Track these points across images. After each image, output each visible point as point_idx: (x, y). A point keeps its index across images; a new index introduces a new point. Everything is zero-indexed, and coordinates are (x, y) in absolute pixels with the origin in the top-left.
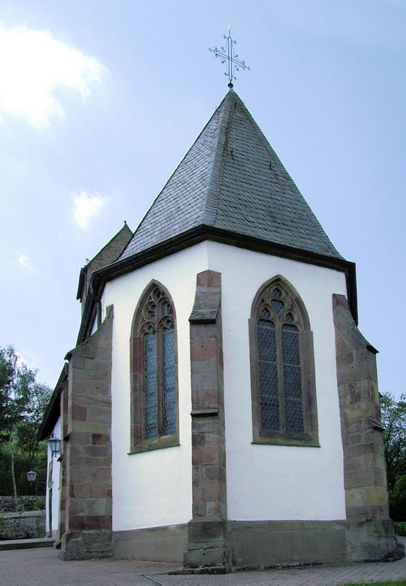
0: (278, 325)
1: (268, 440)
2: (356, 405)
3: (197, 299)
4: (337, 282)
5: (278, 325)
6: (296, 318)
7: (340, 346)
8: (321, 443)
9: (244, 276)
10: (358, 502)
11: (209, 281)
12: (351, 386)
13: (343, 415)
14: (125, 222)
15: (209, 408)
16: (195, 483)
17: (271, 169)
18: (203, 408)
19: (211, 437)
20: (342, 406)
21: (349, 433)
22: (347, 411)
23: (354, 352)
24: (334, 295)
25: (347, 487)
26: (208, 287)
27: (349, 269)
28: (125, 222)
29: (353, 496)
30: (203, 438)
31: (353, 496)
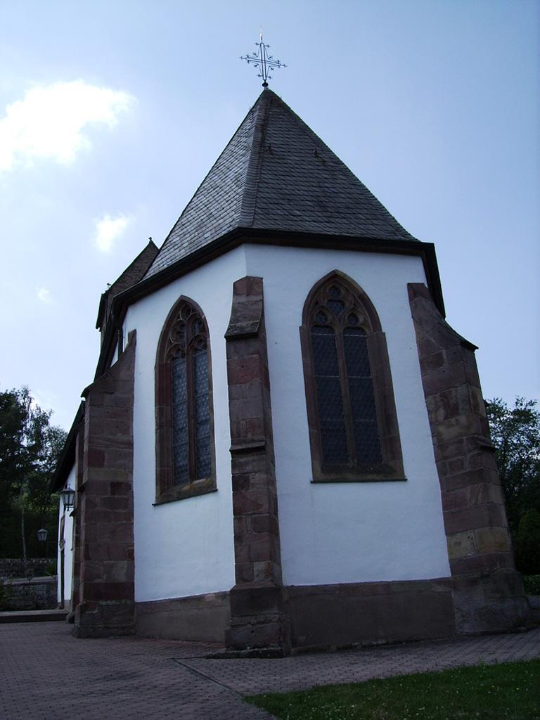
0: (338, 330)
1: (333, 476)
2: (453, 420)
3: (234, 311)
4: (414, 272)
5: (338, 330)
6: (361, 319)
7: (424, 347)
8: (407, 473)
9: (289, 280)
10: (467, 549)
11: (249, 289)
12: (444, 396)
13: (436, 435)
14: (150, 238)
15: (253, 441)
16: (238, 538)
17: (317, 157)
18: (245, 442)
19: (258, 478)
20: (433, 424)
21: (446, 458)
22: (441, 429)
23: (444, 352)
24: (409, 285)
25: (449, 532)
26: (247, 295)
27: (426, 253)
28: (150, 238)
29: (459, 544)
30: (247, 480)
31: (459, 544)
